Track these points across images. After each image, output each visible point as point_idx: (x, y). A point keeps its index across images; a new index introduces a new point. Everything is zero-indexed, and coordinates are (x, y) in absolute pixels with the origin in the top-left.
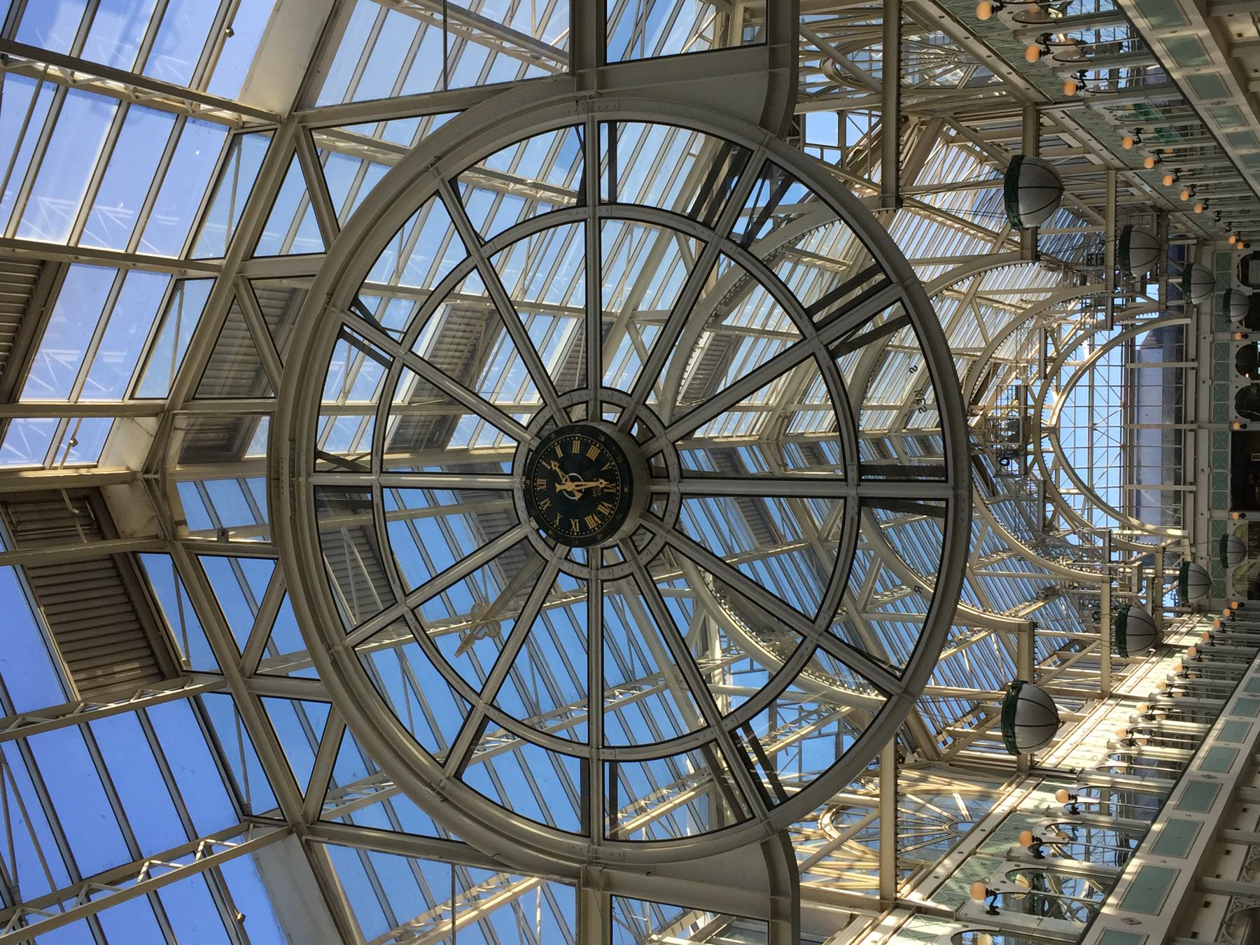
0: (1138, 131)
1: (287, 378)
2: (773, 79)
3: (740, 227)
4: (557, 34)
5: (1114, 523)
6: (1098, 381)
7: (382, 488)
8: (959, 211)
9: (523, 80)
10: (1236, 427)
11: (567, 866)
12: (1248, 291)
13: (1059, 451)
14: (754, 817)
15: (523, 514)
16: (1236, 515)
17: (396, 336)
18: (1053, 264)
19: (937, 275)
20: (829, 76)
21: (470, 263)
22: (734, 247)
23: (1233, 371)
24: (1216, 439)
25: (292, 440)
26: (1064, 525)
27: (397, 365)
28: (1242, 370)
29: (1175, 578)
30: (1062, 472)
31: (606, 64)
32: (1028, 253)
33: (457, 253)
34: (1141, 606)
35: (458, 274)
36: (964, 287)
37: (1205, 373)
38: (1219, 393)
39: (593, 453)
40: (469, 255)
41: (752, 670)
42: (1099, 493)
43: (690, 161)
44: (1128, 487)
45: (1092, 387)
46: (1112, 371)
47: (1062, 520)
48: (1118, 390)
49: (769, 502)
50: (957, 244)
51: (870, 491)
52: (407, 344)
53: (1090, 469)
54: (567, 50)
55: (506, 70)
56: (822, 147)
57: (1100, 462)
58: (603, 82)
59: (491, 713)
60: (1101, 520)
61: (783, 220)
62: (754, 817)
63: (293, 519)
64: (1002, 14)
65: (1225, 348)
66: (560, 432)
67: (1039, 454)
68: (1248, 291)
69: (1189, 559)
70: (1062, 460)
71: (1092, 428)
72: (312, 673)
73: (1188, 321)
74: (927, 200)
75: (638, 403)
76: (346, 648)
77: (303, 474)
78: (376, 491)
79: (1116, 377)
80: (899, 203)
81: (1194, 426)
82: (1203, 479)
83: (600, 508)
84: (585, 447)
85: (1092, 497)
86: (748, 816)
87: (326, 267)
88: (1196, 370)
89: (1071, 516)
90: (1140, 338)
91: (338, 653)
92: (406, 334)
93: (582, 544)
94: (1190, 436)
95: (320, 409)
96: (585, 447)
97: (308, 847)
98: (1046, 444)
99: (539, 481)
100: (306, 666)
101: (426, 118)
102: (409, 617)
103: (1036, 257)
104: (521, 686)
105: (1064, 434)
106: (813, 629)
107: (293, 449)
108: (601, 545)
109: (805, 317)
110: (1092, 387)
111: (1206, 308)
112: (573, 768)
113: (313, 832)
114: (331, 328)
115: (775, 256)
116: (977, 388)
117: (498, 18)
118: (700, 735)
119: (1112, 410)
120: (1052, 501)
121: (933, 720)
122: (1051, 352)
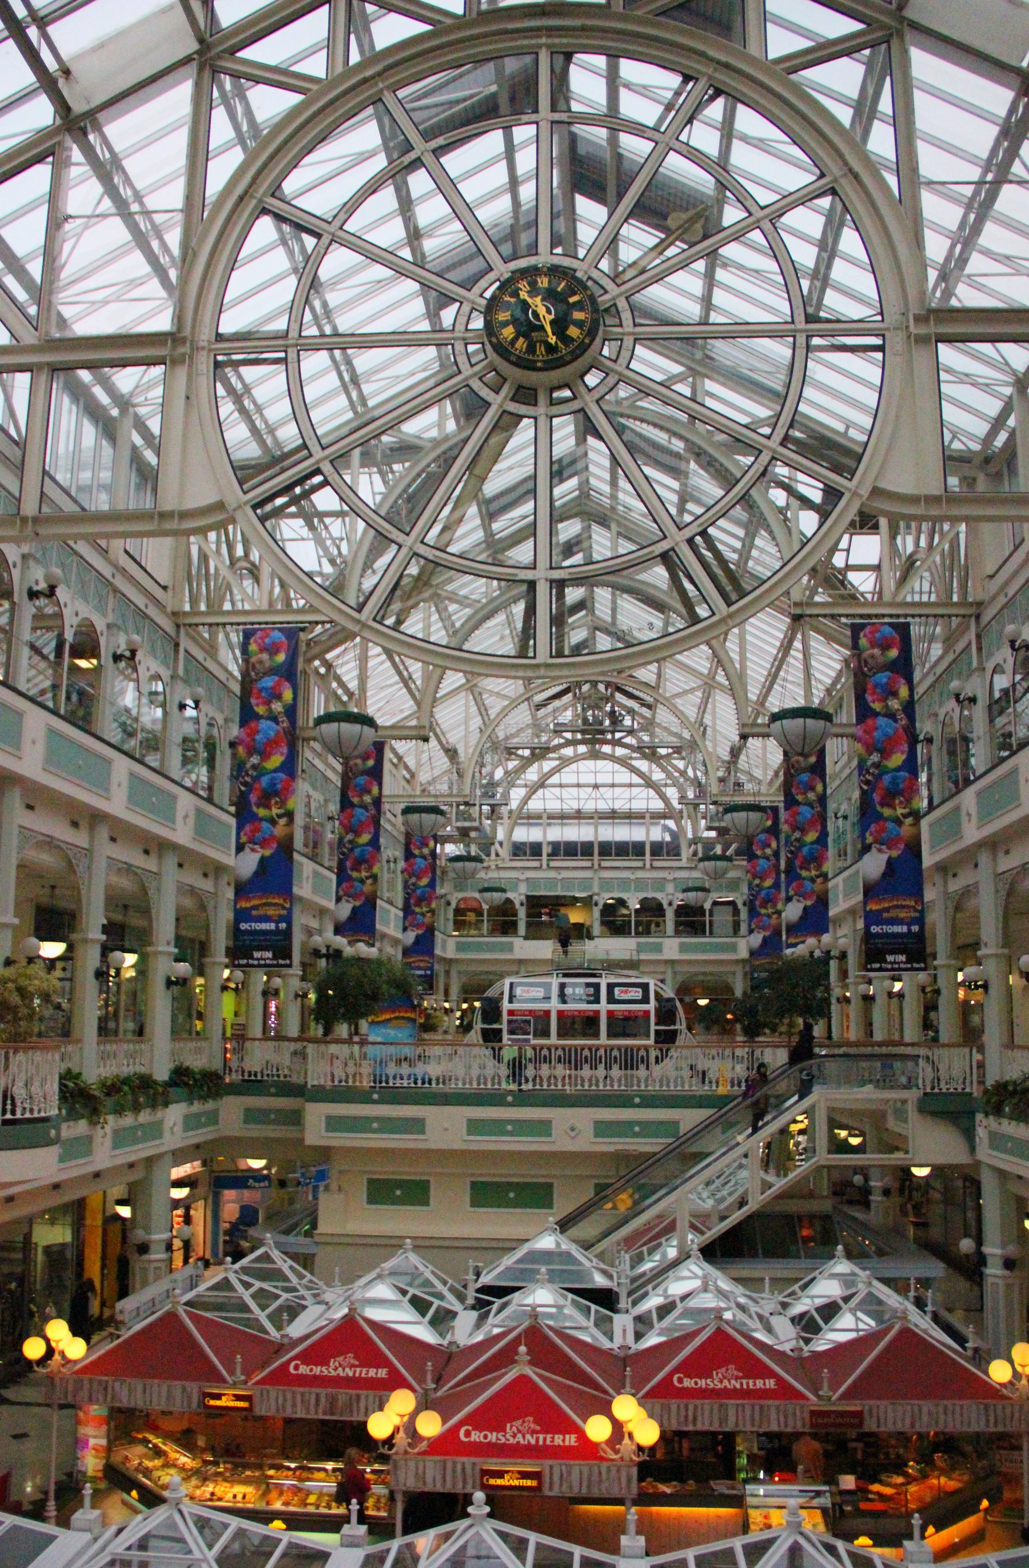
0: (845, 817)
1: (640, 21)
2: (914, 500)
3: (781, 471)
4: (966, 297)
5: (514, 805)
6: (635, 790)
7: (537, 123)
8: (787, 672)
9: (926, 266)
10: (595, 898)
12: (707, 906)
13: (577, 758)
14: (245, 493)
15: (514, 265)
16: (523, 898)
17: (683, 137)
18: (735, 753)
19: (732, 655)
20: (911, 555)
21: (754, 209)
22: (765, 463)
23: (642, 895)
24: (585, 883)
25: (584, 28)
26: (512, 765)
27: (657, 136)
28: (643, 902)
29: (469, 852)
30: (557, 762)
31: (937, 342)
32: (747, 730)
33: (765, 197)
34: (444, 826)
35: (743, 199)
36: (721, 678)
37: (640, 874)
38: (624, 884)
39: (573, 332)
40: (762, 208)
41: (374, 494)
42: (540, 792)
43: (840, 427)
44: (545, 816)
45: (631, 785)
46: (646, 800)
47: (516, 763)
48: (627, 806)
49: (531, 505)
50: (757, 672)
51: (543, 591)
52: (677, 146)
53: (561, 786)
54: (954, 303)
55: (936, 248)
56: (848, 551)
57: (567, 793)
58: (922, 340)
59: (325, 240)
60: (517, 795)
61: (785, 516)
62: (245, 493)
63: (507, 32)
65: (661, 888)
66: (592, 299)
67: (574, 743)
68: (707, 906)
69: (485, 864)
70: (566, 762)
71: (596, 786)
72: (355, 58)
73: (684, 860)
74: (797, 644)
75: (620, 374)
77: (550, 41)
78: (534, 117)
79: (638, 805)
80: (797, 618)
81: (596, 866)
82: (552, 874)
83: (521, 340)
84: (579, 324)
85: (534, 789)
86: (245, 487)
87: (753, 61)
88: (643, 868)
89: (521, 769)
90: (671, 824)
91: (376, 84)
92: (687, 144)
93: (488, 324)
94: (588, 864)
95: (613, 57)
96: (579, 324)
97: (186, 61)
98: (582, 749)
99: (546, 280)
100: (362, 51)
101: (894, 167)
102: (412, 156)
103: (744, 737)
104: (354, 271)
105: (590, 764)
106: (415, 542)
107: (574, 29)
108: (487, 343)
109: (700, 529)
110: (631, 785)
111: (696, 874)
112: (280, 324)
114: (693, 65)
115: (751, 507)
116: (631, 690)
117: (983, 240)
119: (610, 802)
120: (533, 754)
121: (338, 657)
122: (663, 751)
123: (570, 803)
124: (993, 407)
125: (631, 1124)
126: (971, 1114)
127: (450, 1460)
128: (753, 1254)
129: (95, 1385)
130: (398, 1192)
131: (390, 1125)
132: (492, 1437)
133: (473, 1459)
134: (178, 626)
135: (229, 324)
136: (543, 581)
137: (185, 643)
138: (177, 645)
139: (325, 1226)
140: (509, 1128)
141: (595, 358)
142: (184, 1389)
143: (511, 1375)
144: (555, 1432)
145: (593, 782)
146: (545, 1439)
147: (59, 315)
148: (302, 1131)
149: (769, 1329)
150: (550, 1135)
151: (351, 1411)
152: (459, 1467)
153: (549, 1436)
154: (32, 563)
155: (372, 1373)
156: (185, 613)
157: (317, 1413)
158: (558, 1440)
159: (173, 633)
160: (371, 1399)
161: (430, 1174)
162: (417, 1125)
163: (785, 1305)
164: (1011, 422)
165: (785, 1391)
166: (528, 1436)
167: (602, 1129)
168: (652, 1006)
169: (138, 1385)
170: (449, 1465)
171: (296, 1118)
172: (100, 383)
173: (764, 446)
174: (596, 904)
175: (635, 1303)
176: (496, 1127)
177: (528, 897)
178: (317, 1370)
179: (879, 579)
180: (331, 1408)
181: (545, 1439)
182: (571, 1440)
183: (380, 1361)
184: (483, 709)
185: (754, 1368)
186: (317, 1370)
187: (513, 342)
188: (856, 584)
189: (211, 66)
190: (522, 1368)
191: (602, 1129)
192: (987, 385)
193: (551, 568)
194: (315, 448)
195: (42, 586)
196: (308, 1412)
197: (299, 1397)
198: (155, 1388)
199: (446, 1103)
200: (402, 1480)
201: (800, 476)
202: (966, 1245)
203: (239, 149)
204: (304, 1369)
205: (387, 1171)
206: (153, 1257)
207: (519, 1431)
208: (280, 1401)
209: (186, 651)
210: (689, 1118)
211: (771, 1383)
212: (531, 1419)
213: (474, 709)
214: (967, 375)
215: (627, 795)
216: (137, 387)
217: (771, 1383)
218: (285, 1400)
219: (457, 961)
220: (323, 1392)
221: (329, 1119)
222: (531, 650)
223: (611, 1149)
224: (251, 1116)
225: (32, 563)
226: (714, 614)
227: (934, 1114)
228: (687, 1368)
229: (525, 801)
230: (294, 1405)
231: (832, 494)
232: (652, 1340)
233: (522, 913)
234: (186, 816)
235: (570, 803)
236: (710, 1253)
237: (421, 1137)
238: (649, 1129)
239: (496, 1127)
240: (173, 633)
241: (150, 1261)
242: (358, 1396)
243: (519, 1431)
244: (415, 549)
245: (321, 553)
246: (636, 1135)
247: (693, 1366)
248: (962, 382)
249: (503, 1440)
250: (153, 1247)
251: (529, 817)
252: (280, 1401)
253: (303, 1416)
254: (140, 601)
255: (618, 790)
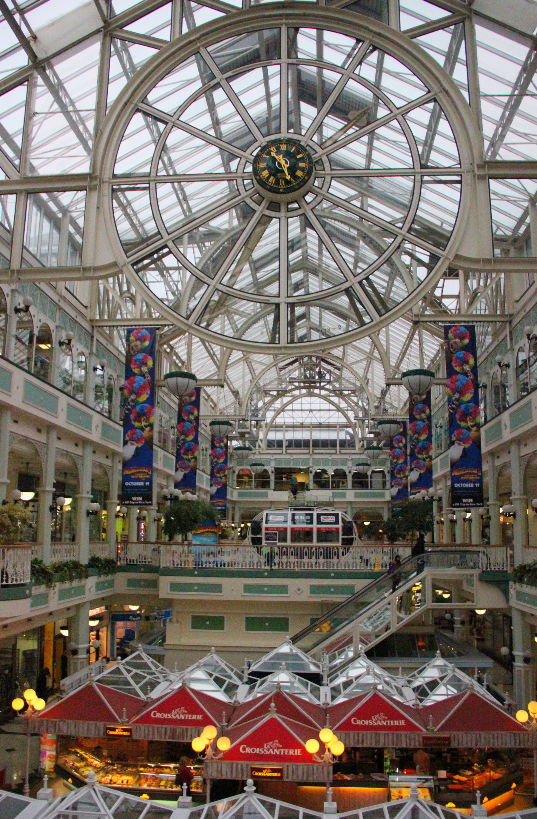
0: (441, 427)
1: (334, 11)
3: (408, 246)
4: (504, 155)
5: (268, 420)
6: (331, 413)
7: (280, 64)
8: (411, 351)
9: (483, 139)
10: (311, 469)
11: (320, 790)
12: (369, 473)
13: (301, 396)
14: (128, 257)
15: (268, 138)
16: (273, 469)
17: (357, 72)
18: (384, 393)
19: (382, 342)
20: (475, 290)
21: (393, 109)
22: (399, 242)
23: (335, 468)
24: (305, 461)
25: (305, 15)
26: (267, 399)
27: (343, 71)
28: (336, 471)
29: (245, 445)
30: (291, 398)
31: (489, 178)
32: (390, 381)
33: (399, 103)
35: (388, 104)
36: (376, 354)
37: (334, 457)
38: (326, 462)
39: (299, 173)
40: (398, 109)
41: (195, 258)
42: (282, 414)
43: (439, 223)
44: (284, 426)
45: (329, 410)
46: (337, 418)
47: (269, 398)
48: (327, 421)
49: (277, 264)
50: (395, 351)
51: (283, 309)
52: (353, 76)
53: (293, 410)
54: (498, 158)
55: (489, 129)
56: (443, 288)
57: (296, 414)
58: (481, 178)
59: (170, 125)
60: (270, 415)
61: (410, 269)
62: (128, 257)
63: (264, 17)
64: (497, 367)
65: (345, 464)
66: (309, 156)
67: (299, 388)
68: (369, 473)
70: (295, 398)
71: (311, 411)
72: (185, 30)
73: (357, 449)
74: (416, 337)
75: (324, 195)
76: (199, 48)
77: (287, 21)
78: (279, 61)
79: (333, 421)
81: (311, 452)
82: (288, 457)
83: (272, 178)
84: (302, 169)
85: (278, 412)
86: (128, 254)
87: (393, 32)
88: (336, 453)
89: (272, 402)
91: (196, 44)
92: (359, 75)
93: (255, 169)
94: (307, 451)
95: (320, 30)
96: (302, 169)
97: (97, 32)
98: (304, 391)
99: (285, 146)
100: (189, 27)
101: (467, 87)
103: (388, 385)
104: (185, 141)
105: (308, 399)
106: (217, 283)
107: (299, 15)
108: (254, 179)
109: (365, 277)
110: (329, 410)
111: (363, 457)
112: (146, 169)
113: (105, 36)
114: (362, 34)
115: (392, 265)
116: (329, 360)
117: (513, 126)
118: (155, 171)
119: (318, 419)
120: (278, 394)
121: (176, 343)
122: (346, 392)
123: (298, 419)
124: (518, 213)
125: (329, 587)
126: (507, 582)
127: (235, 763)
128: (393, 655)
129: (50, 723)
130: (208, 623)
131: (203, 588)
132: (257, 751)
133: (247, 762)
134: (93, 327)
135: (120, 169)
136: (283, 304)
137: (96, 336)
138: (92, 337)
139: (170, 641)
140: (266, 589)
141: (311, 187)
142: (96, 726)
143: (267, 718)
144: (289, 748)
145: (309, 408)
146: (284, 752)
147: (31, 164)
148: (158, 591)
149: (401, 694)
150: (287, 593)
151: (183, 737)
152: (240, 766)
153: (286, 750)
154: (16, 294)
155: (194, 717)
156: (97, 320)
157: (165, 738)
158: (291, 752)
159: (90, 331)
160: (193, 731)
161: (224, 613)
162: (218, 588)
163: (409, 682)
164: (528, 220)
165: (409, 727)
166: (276, 750)
167: (314, 590)
168: (340, 525)
169: (72, 723)
170: (234, 765)
171: (154, 584)
172: (52, 200)
173: (399, 233)
174: (311, 472)
175: (331, 681)
176: (259, 589)
177: (275, 469)
178: (166, 716)
179: (459, 302)
180: (173, 735)
181: (284, 752)
182: (298, 752)
183: (198, 711)
184: (252, 371)
185: (393, 715)
186: (166, 716)
187: (268, 179)
188: (447, 305)
189: (110, 34)
190: (272, 715)
191: (314, 590)
192: (515, 201)
193: (288, 297)
194: (164, 234)
195: (22, 306)
196: (161, 738)
197: (156, 730)
198: (81, 725)
199: (233, 576)
200: (210, 773)
201: (418, 249)
202: (504, 650)
203: (125, 78)
204: (159, 715)
205: (202, 612)
206: (80, 656)
207: (271, 748)
208: (146, 732)
209: (97, 340)
210: (360, 584)
211: (402, 723)
212: (277, 741)
213: (247, 370)
214: (505, 196)
215: (327, 415)
216: (72, 202)
217: (402, 723)
218: (149, 731)
219: (238, 502)
220: (169, 727)
221: (172, 584)
222: (277, 339)
223: (319, 600)
224: (131, 583)
225: (16, 294)
226: (372, 321)
227: (488, 582)
228: (358, 714)
229: (274, 418)
230: (153, 734)
231: (434, 258)
232: (340, 700)
233: (272, 477)
234: (97, 426)
235: (298, 419)
236: (370, 654)
237: (220, 594)
238: (338, 589)
239: (259, 589)
240: (90, 331)
241: (78, 659)
242: (187, 729)
243: (271, 748)
244: (217, 287)
245: (168, 289)
246: (332, 593)
247: (362, 714)
248: (502, 200)
249: (263, 752)
250: (80, 651)
251: (276, 427)
252: (146, 732)
253: (158, 740)
254: (73, 314)
255: (322, 413)
